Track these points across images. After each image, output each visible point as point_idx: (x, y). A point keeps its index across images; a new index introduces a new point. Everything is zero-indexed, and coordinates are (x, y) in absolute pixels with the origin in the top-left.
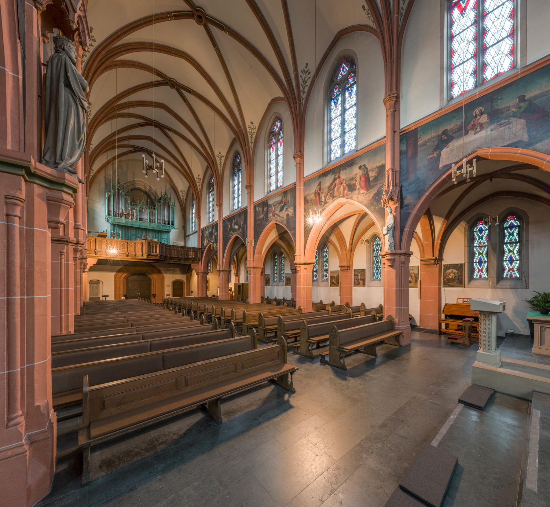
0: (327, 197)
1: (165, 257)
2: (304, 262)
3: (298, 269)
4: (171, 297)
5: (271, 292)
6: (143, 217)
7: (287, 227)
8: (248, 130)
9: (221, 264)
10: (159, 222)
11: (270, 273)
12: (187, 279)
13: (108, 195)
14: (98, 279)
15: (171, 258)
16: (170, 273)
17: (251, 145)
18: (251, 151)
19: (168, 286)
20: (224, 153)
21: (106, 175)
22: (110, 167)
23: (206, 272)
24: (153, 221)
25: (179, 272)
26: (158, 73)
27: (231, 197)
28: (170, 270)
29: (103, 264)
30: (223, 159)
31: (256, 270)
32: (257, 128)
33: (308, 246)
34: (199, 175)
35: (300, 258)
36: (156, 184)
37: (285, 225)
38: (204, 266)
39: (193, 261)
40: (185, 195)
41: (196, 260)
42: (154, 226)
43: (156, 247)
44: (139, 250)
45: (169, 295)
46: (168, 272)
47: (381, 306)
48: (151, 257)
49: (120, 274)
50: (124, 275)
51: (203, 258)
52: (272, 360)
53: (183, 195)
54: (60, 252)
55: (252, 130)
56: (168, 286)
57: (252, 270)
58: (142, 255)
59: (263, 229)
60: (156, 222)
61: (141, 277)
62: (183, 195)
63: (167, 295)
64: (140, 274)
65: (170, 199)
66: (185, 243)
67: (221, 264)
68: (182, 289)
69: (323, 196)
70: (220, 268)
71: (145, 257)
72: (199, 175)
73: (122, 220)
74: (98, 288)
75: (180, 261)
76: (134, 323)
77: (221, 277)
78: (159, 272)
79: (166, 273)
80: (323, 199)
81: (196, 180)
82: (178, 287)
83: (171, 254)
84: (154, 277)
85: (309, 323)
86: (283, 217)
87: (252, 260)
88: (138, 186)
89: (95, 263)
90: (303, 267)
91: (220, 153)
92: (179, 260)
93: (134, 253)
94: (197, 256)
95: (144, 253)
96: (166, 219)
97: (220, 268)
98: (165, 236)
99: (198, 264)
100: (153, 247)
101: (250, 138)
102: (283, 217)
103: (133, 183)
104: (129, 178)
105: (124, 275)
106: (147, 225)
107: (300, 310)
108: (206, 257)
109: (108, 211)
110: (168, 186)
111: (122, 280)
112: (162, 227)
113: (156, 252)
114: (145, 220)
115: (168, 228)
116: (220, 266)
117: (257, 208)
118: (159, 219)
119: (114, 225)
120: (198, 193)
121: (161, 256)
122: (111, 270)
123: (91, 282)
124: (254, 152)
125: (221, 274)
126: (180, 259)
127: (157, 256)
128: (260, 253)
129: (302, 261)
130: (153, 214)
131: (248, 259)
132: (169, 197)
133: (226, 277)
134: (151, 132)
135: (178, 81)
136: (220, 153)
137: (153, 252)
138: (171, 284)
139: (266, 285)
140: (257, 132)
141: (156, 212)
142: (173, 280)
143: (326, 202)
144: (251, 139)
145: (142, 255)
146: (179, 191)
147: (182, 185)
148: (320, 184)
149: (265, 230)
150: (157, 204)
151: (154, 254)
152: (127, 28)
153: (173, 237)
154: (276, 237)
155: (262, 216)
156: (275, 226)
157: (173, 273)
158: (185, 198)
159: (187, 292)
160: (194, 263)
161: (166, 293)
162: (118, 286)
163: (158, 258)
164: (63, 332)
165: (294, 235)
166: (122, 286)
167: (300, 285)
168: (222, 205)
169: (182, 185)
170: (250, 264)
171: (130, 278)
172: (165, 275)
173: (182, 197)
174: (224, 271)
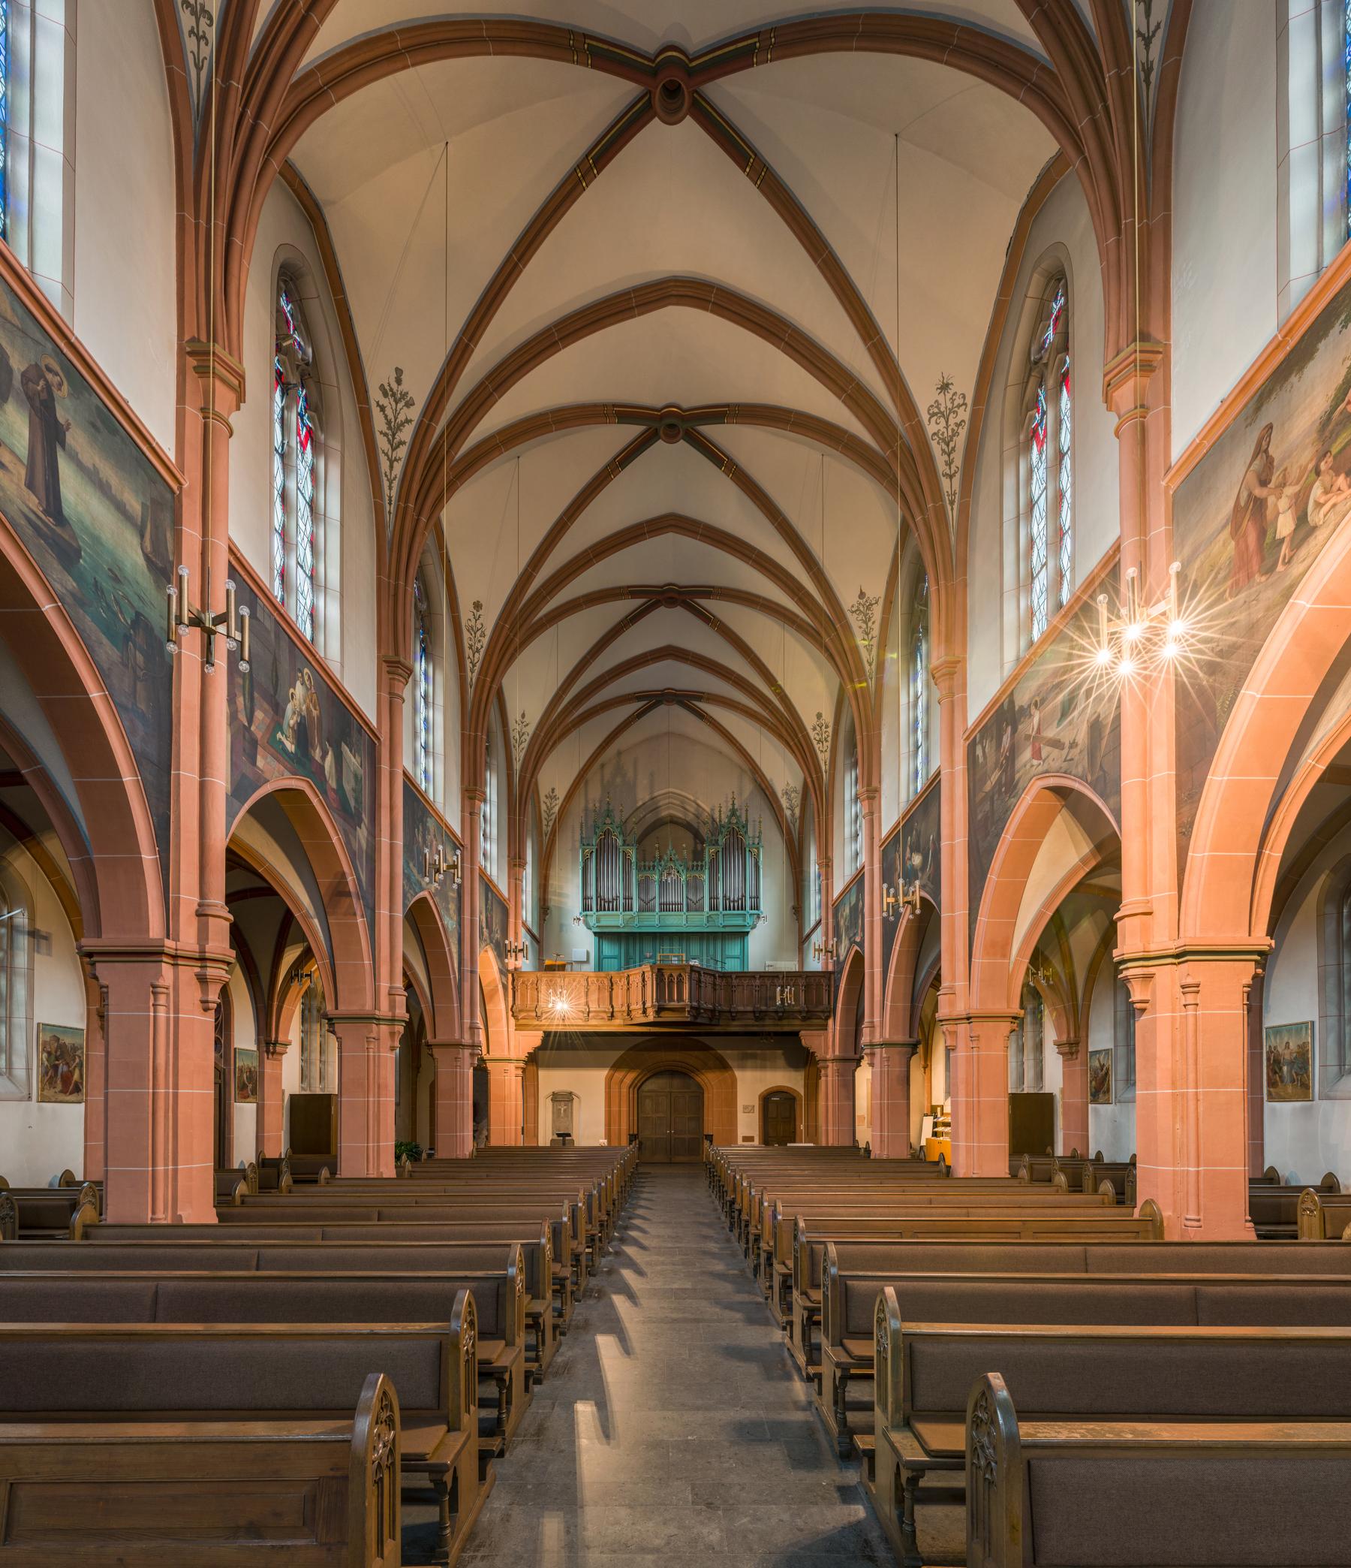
0: (1317, 492)
1: (713, 1011)
2: (1173, 947)
3: (1137, 994)
4: (756, 1142)
5: (1117, 1132)
6: (671, 898)
7: (1093, 786)
8: (931, 428)
9: (877, 1020)
10: (713, 907)
11: (1110, 1045)
12: (807, 1086)
13: (584, 856)
14: (569, 1090)
15: (733, 1015)
16: (755, 1068)
17: (950, 486)
18: (953, 514)
19: (748, 1109)
20: (877, 590)
21: (587, 801)
22: (594, 776)
23: (851, 1055)
24: (695, 907)
25: (781, 1062)
26: (624, 413)
27: (904, 749)
28: (754, 1057)
29: (560, 1048)
30: (877, 612)
31: (978, 1027)
32: (969, 401)
33: (1199, 853)
34: (819, 716)
35: (1146, 931)
36: (710, 794)
37: (1083, 778)
38: (844, 1035)
39: (804, 1019)
40: (797, 800)
41: (816, 1015)
42: (696, 922)
43: (680, 982)
44: (635, 1001)
45: (751, 1139)
46: (749, 1062)
47: (68, 1178)
48: (668, 1017)
49: (619, 1075)
50: (631, 1076)
51: (839, 1005)
52: (254, 1530)
53: (789, 805)
54: (154, 987)
55: (942, 428)
56: (748, 1109)
57: (962, 1028)
58: (644, 1012)
59: (998, 836)
60: (706, 909)
61: (677, 1082)
62: (789, 805)
63: (746, 1139)
64: (672, 1072)
65: (745, 826)
66: (802, 962)
67: (877, 1020)
68: (791, 1119)
69: (1283, 503)
70: (872, 1034)
71: (651, 1017)
72: (819, 716)
73: (615, 920)
74: (569, 1114)
75: (776, 1020)
76: (385, 1210)
77: (877, 1069)
78: (723, 1066)
79: (742, 1067)
80: (1285, 525)
81: (812, 734)
82: (780, 1116)
83: (731, 1002)
84: (710, 1080)
85: (914, 1306)
86: (1073, 745)
87: (960, 984)
88: (664, 814)
89: (538, 1042)
90: (1168, 977)
91: (862, 595)
92: (757, 1019)
93: (625, 1008)
94: (820, 1002)
95: (648, 1004)
96: (734, 895)
97: (872, 1034)
98: (733, 948)
99: (825, 1027)
100: (671, 982)
101: (940, 460)
102: (1073, 745)
103: (653, 805)
104: (642, 796)
105: (631, 1076)
106: (677, 921)
107: (1153, 1224)
108: (846, 1003)
109: (585, 898)
110: (748, 787)
111: (624, 1090)
112: (723, 921)
113: (680, 998)
114: (677, 907)
115: (741, 922)
116: (872, 1026)
117: (979, 752)
118: (713, 898)
119: (601, 936)
120: (820, 778)
121: (696, 1010)
122: (598, 1065)
123: (556, 1097)
124: (965, 512)
125: (877, 1060)
126: (759, 1015)
127: (681, 1010)
128: (1002, 947)
129: (1162, 940)
130: (695, 885)
131: (945, 983)
132: (743, 819)
133: (898, 1070)
134: (668, 627)
135: (685, 405)
136: (862, 595)
137: (671, 999)
138: (756, 1103)
139: (1095, 1099)
140: (975, 415)
141: (706, 877)
142: (762, 1089)
143: (1304, 528)
144: (946, 462)
145: (644, 1012)
146: (779, 795)
147: (783, 773)
148: (1261, 450)
149: (1008, 837)
150: (709, 851)
151: (674, 1004)
152: (478, 317)
153: (761, 948)
154: (1084, 861)
155: (994, 777)
156: (1053, 800)
157: (763, 1067)
158: (797, 811)
159: (807, 1127)
160: (809, 1028)
161: (742, 1131)
162: (615, 1109)
163: (686, 1017)
164: (160, 1215)
165: (1117, 814)
166: (624, 1109)
167: (1151, 1084)
168: (877, 790)
169: (783, 773)
170: (952, 1004)
171: (650, 1086)
172: (738, 1074)
173: (788, 813)
174: (885, 1045)
